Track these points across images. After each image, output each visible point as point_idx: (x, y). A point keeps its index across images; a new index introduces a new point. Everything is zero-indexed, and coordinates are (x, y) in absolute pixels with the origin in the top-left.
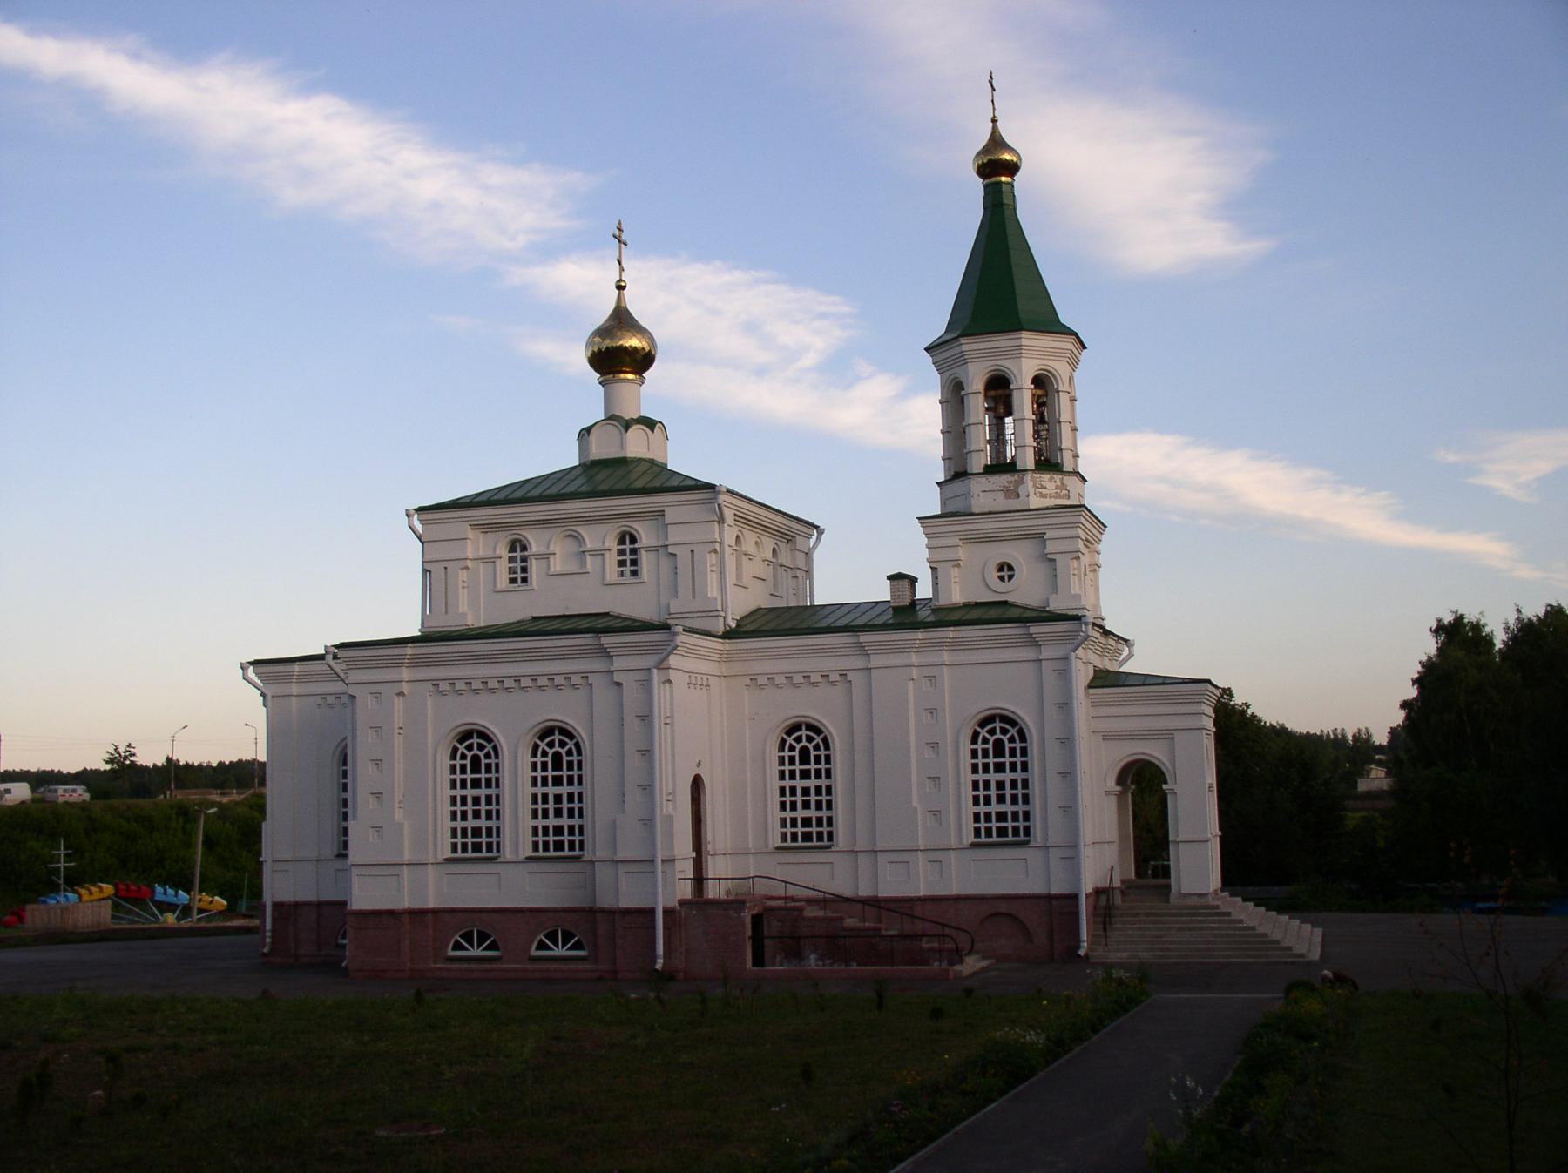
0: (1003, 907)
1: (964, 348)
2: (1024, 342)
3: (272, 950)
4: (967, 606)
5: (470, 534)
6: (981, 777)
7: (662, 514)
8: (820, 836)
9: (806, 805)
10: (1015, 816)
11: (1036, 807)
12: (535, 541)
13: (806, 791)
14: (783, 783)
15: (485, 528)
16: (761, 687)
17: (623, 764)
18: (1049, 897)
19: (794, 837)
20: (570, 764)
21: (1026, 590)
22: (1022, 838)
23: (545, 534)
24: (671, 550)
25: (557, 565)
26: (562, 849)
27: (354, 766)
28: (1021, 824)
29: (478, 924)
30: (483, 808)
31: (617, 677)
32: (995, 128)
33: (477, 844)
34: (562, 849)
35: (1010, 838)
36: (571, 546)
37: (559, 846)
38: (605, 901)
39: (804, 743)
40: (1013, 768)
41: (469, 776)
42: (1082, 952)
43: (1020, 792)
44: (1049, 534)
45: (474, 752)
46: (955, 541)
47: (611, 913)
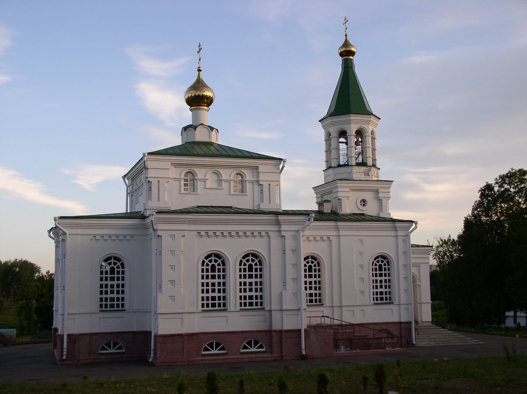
0: (384, 327)
1: (352, 118)
2: (352, 118)
3: (67, 358)
4: (350, 215)
5: (172, 168)
6: (205, 281)
7: (257, 168)
8: (118, 306)
9: (112, 292)
10: (219, 298)
11: (266, 293)
12: (200, 173)
13: (251, 284)
14: (102, 282)
15: (176, 165)
16: (310, 241)
17: (285, 271)
18: (401, 323)
19: (208, 305)
20: (385, 269)
21: (371, 210)
22: (318, 303)
23: (229, 171)
24: (261, 183)
25: (209, 184)
26: (313, 302)
27: (369, 267)
28: (259, 301)
29: (217, 339)
30: (379, 284)
31: (283, 233)
32: (346, 38)
33: (215, 303)
34: (313, 302)
35: (217, 308)
36: (215, 177)
37: (214, 305)
38: (276, 326)
39: (310, 264)
40: (118, 279)
41: (247, 273)
42: (150, 360)
43: (222, 287)
44: (380, 190)
45: (214, 263)
46: (348, 190)
47: (281, 332)
